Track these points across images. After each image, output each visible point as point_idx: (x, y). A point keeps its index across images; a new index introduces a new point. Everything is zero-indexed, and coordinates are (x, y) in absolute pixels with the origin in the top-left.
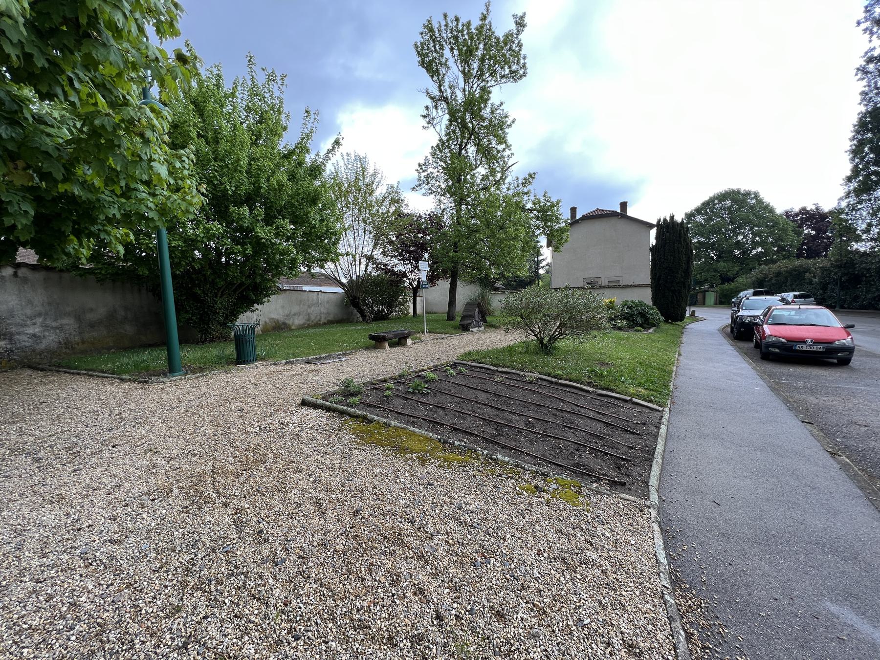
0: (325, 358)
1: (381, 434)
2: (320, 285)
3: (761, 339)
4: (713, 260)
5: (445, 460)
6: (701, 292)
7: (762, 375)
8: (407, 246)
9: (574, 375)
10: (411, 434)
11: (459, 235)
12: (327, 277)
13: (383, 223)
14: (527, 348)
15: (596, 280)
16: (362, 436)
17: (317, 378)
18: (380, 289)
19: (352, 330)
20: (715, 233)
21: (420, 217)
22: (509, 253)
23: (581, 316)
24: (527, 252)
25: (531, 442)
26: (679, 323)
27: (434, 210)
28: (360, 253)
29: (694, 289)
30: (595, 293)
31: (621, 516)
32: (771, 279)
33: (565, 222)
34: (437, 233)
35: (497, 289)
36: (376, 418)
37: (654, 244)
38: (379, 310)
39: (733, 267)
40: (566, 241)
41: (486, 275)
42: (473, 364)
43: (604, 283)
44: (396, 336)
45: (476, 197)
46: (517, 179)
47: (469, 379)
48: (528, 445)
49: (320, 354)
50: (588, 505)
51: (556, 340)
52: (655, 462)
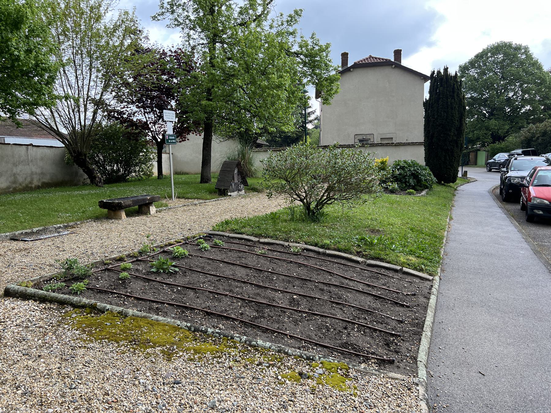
0: (38, 232)
1: (114, 326)
2: (30, 136)
3: (527, 202)
4: (485, 117)
5: (196, 352)
6: (473, 151)
7: (527, 238)
8: (147, 90)
9: (342, 245)
10: (152, 324)
11: (213, 79)
12: (38, 124)
13: (116, 58)
14: (293, 215)
15: (368, 137)
16: (90, 331)
17: (26, 260)
18: (114, 144)
19: (76, 196)
20: (488, 88)
21: (164, 53)
22: (273, 104)
23: (351, 179)
24: (293, 104)
25: (296, 322)
26: (451, 184)
27: (181, 47)
28: (85, 96)
29: (467, 148)
30: (366, 151)
31: (389, 397)
32: (538, 138)
33: (335, 69)
34: (186, 75)
35: (259, 146)
36: (108, 306)
37: (428, 98)
38: (112, 169)
39: (503, 125)
40: (336, 92)
41: (247, 129)
42: (231, 235)
43: (377, 140)
44: (135, 203)
45: (232, 34)
46: (282, 15)
47: (226, 253)
48: (293, 326)
49: (30, 228)
50: (355, 388)
51: (323, 206)
52: (424, 335)
